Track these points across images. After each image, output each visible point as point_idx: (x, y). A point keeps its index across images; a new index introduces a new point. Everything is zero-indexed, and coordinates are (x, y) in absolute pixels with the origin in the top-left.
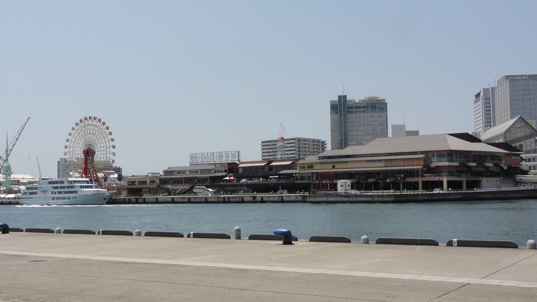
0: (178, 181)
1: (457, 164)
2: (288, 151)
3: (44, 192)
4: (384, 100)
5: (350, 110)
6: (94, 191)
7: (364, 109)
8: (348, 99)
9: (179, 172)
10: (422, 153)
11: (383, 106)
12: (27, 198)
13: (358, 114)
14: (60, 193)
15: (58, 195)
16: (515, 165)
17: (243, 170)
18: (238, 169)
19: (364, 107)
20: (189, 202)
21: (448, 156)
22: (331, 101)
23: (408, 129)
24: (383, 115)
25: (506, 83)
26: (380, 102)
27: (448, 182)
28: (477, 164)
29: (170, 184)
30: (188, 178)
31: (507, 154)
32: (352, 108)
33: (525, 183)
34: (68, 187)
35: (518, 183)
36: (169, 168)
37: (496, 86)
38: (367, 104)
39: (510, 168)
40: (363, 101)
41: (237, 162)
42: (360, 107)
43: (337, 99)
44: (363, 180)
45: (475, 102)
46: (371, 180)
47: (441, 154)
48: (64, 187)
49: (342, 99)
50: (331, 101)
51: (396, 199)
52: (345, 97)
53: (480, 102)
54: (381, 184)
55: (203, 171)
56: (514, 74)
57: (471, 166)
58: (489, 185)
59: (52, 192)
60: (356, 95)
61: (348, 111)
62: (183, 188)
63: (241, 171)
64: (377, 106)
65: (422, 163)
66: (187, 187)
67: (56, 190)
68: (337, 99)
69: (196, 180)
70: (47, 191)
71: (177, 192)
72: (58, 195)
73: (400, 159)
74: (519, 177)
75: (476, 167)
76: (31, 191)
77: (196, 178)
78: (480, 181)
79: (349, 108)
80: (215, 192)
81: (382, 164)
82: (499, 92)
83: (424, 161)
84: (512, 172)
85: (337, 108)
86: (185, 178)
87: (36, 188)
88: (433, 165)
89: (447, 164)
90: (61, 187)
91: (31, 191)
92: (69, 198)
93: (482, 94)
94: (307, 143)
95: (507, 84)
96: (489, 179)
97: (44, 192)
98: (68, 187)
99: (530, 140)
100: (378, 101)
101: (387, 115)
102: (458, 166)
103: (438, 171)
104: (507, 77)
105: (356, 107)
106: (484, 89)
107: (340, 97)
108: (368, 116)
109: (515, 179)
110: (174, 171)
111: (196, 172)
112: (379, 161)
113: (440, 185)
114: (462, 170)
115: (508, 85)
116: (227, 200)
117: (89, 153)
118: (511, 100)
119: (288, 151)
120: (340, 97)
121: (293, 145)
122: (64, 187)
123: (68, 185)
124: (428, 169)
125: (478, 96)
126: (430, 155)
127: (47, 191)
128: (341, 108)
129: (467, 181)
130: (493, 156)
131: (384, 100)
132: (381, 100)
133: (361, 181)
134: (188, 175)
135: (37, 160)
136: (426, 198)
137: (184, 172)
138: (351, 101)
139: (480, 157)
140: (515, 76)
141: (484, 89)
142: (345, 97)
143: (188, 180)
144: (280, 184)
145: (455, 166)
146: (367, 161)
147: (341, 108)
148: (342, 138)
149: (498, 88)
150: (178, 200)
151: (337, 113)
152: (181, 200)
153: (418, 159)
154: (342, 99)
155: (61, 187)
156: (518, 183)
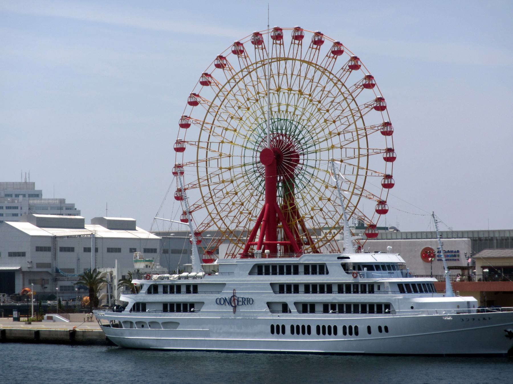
3: (234, 302)
4: (74, 204)
6: (458, 305)
12: (153, 324)
14: (307, 308)
15: (295, 317)
34: (347, 288)
48: (328, 288)
59: (269, 304)
67: (290, 298)
70: (248, 301)
72: (295, 317)
76: (455, 258)
87: (193, 289)
90: (310, 288)
91: (455, 258)
92: (351, 330)
97: (234, 302)
98: (347, 288)
117: (279, 162)
122: (328, 288)
123: (349, 279)
127: (248, 301)
131: (74, 204)
135: (3, 195)
155: (310, 288)
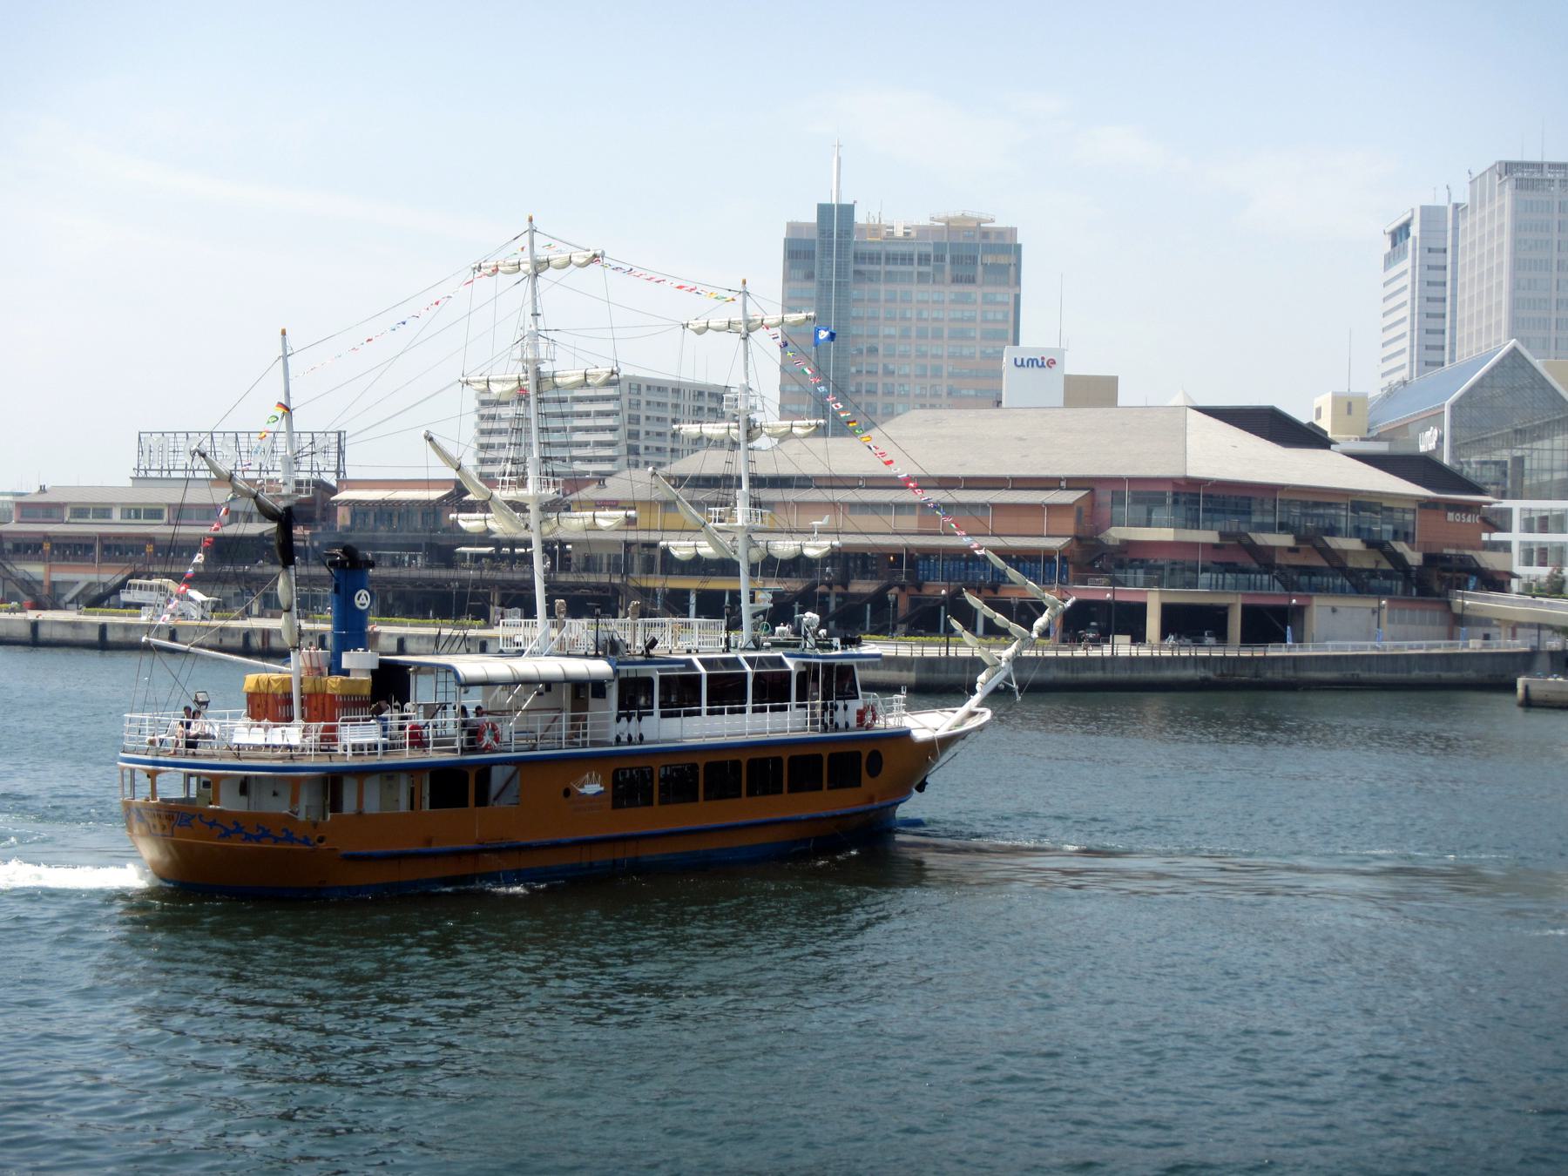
0: (75, 549)
1: (1211, 537)
2: (587, 430)
4: (1013, 231)
5: (863, 267)
7: (923, 269)
8: (860, 218)
9: (80, 511)
10: (1073, 483)
11: (1003, 260)
13: (899, 288)
16: (1458, 547)
17: (354, 515)
18: (329, 510)
19: (924, 259)
20: (103, 644)
21: (1176, 502)
22: (792, 227)
23: (1075, 365)
24: (1003, 294)
25: (1501, 193)
26: (993, 240)
27: (1168, 611)
28: (1298, 539)
29: (41, 560)
30: (119, 537)
31: (1426, 505)
32: (873, 258)
33: (1483, 623)
35: (1459, 622)
36: (43, 490)
37: (1462, 196)
38: (937, 245)
39: (1431, 559)
40: (923, 231)
41: (331, 479)
42: (906, 259)
43: (812, 218)
44: (830, 585)
45: (1390, 260)
46: (862, 587)
47: (1151, 494)
49: (836, 218)
50: (792, 227)
51: (924, 676)
52: (847, 211)
53: (1406, 264)
54: (904, 606)
55: (180, 512)
56: (1536, 158)
57: (1273, 548)
58: (1340, 629)
60: (894, 207)
61: (857, 272)
62: (93, 577)
63: (343, 518)
64: (977, 259)
65: (1069, 525)
66: (109, 576)
68: (815, 220)
69: (150, 549)
71: (70, 596)
73: (984, 506)
74: (1472, 601)
75: (1291, 550)
77: (150, 539)
78: (1300, 611)
79: (860, 257)
80: (216, 607)
81: (910, 522)
82: (1473, 225)
83: (1078, 521)
84: (1441, 578)
85: (810, 255)
86: (103, 537)
88: (1117, 534)
89: (1166, 534)
93: (1415, 230)
94: (670, 399)
95: (1506, 198)
96: (1341, 602)
99: (1547, 444)
100: (986, 234)
101: (1017, 298)
102: (1215, 546)
103: (1128, 559)
104: (1509, 168)
105: (892, 258)
106: (1423, 208)
107: (824, 211)
108: (932, 301)
109: (1449, 604)
110: (60, 506)
111: (154, 513)
112: (900, 507)
113: (1130, 620)
114: (1240, 557)
115: (1507, 200)
116: (256, 642)
118: (1518, 265)
119: (587, 430)
120: (824, 211)
121: (609, 407)
124: (1089, 555)
125: (1400, 234)
126: (1104, 496)
128: (829, 254)
129: (1246, 609)
130: (1361, 503)
131: (1013, 231)
132: (1001, 233)
133: (820, 589)
134: (118, 526)
136: (1061, 675)
137: (103, 511)
138: (875, 230)
139: (1311, 509)
140: (1539, 166)
141: (1423, 208)
142: (847, 211)
143: (114, 548)
144: (492, 583)
145: (1205, 545)
146: (853, 506)
147: (829, 254)
148: (836, 374)
149: (1473, 212)
150: (59, 634)
151: (810, 276)
152: (68, 634)
153: (1052, 508)
154: (836, 218)
156: (1459, 622)
